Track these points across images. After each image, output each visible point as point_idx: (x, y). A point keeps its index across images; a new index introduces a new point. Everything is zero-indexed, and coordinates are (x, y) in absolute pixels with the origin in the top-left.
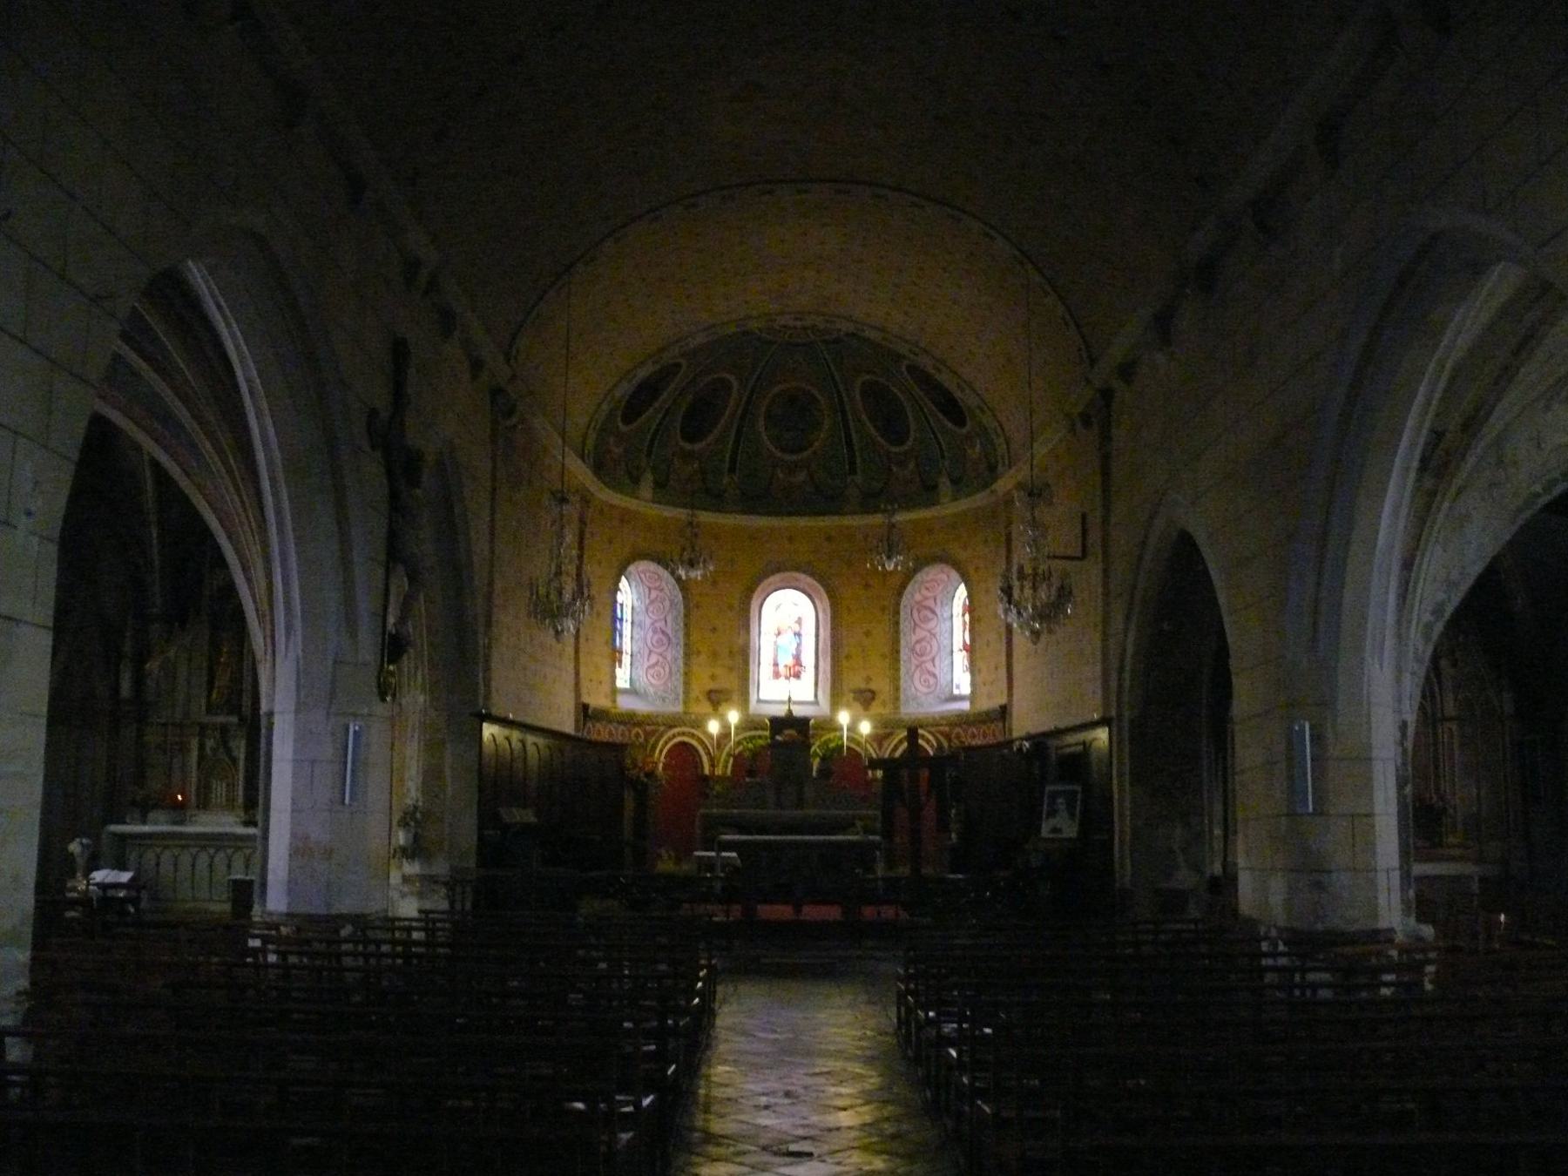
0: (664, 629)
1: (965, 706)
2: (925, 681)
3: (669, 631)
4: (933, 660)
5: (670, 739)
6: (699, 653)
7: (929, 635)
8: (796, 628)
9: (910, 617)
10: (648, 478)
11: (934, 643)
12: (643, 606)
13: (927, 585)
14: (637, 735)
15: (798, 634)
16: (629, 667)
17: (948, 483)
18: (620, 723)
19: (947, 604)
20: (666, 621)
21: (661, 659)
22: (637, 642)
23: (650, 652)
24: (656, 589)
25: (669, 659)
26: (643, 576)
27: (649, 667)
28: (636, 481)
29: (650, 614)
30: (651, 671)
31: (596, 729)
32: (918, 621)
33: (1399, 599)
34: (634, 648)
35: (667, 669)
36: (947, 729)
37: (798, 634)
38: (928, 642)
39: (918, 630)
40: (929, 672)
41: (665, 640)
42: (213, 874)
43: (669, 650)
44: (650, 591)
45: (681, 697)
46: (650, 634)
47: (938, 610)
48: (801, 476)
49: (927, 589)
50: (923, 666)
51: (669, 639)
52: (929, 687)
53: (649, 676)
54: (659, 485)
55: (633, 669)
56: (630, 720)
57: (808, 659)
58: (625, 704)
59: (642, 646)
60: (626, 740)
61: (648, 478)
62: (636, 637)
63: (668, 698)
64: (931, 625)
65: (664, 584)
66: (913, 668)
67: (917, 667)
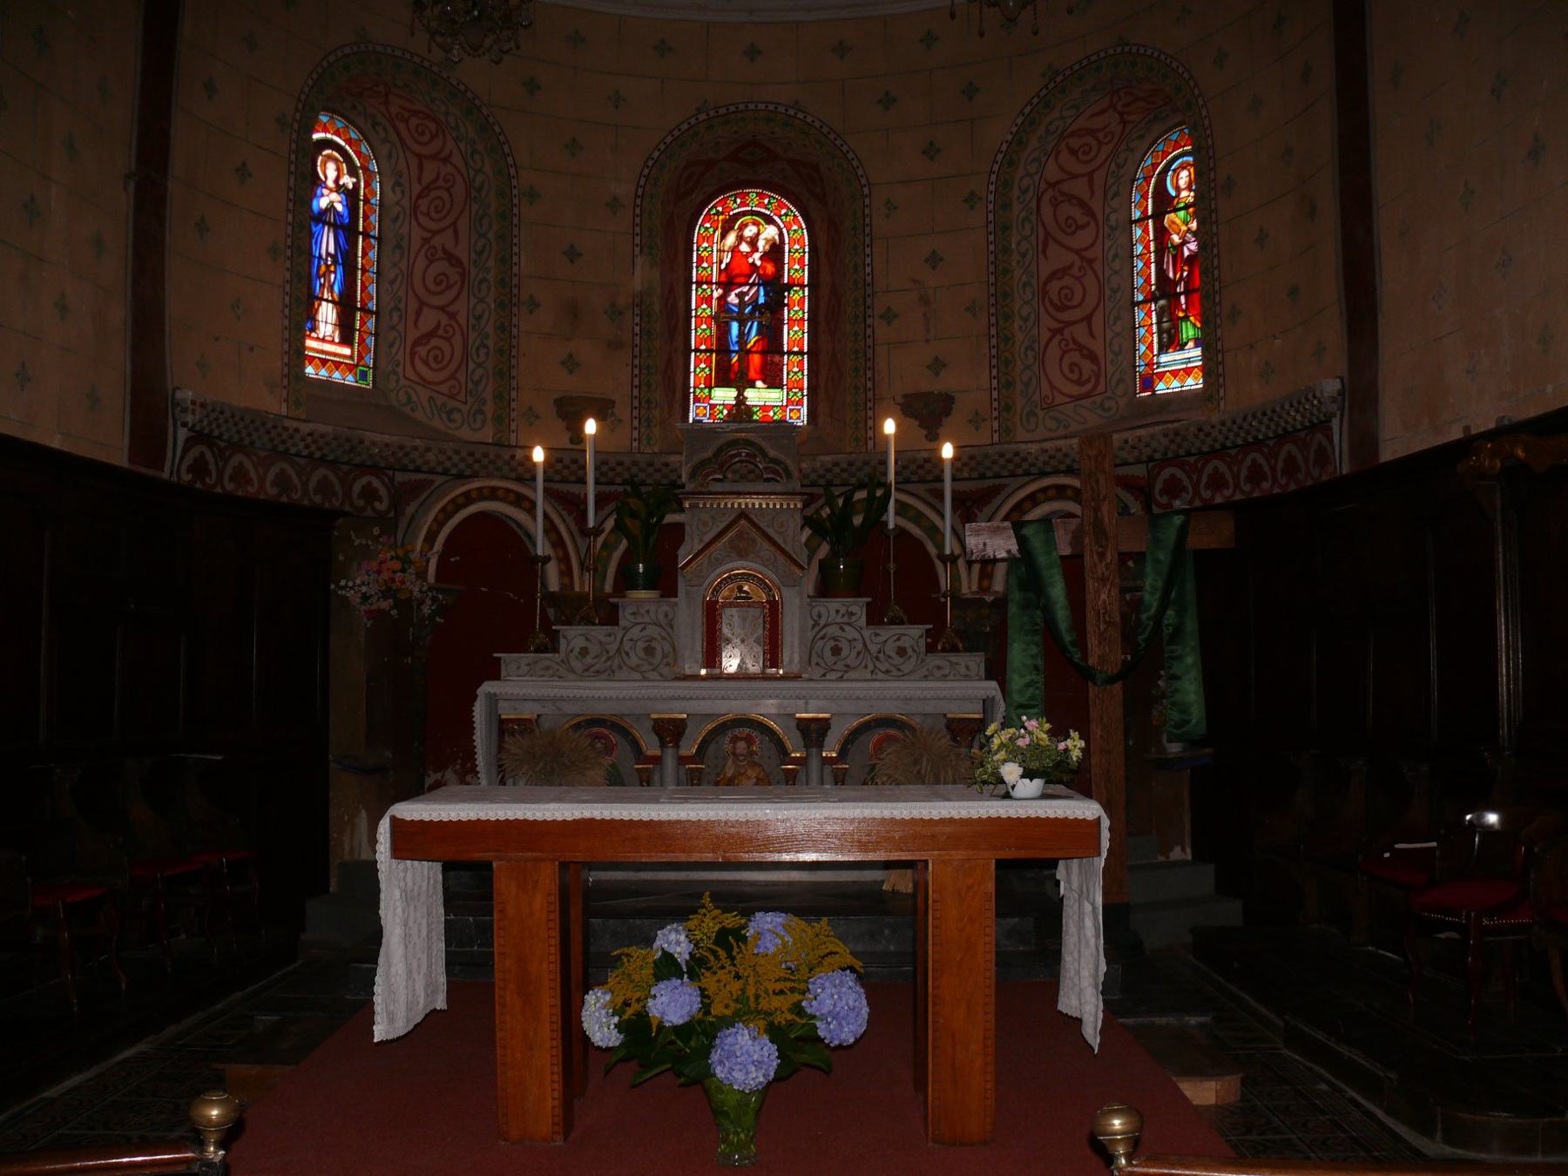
2: (1072, 371)
5: (456, 506)
6: (534, 305)
7: (1078, 263)
9: (1033, 218)
12: (405, 202)
13: (1075, 143)
14: (370, 494)
16: (371, 341)
19: (1116, 194)
20: (456, 232)
21: (445, 320)
22: (392, 282)
23: (422, 304)
24: (434, 157)
25: (462, 319)
26: (402, 126)
27: (417, 342)
29: (422, 219)
30: (422, 351)
31: (594, 661)
33: (438, 785)
35: (457, 340)
36: (1140, 471)
38: (1078, 279)
39: (1052, 247)
40: (1080, 347)
42: (700, 697)
44: (421, 167)
45: (489, 408)
46: (421, 263)
47: (1096, 205)
49: (1073, 152)
50: (1067, 332)
51: (463, 275)
52: (1079, 383)
53: (418, 362)
59: (402, 293)
63: (459, 411)
64: (1082, 239)
66: (1045, 335)
67: (1054, 332)
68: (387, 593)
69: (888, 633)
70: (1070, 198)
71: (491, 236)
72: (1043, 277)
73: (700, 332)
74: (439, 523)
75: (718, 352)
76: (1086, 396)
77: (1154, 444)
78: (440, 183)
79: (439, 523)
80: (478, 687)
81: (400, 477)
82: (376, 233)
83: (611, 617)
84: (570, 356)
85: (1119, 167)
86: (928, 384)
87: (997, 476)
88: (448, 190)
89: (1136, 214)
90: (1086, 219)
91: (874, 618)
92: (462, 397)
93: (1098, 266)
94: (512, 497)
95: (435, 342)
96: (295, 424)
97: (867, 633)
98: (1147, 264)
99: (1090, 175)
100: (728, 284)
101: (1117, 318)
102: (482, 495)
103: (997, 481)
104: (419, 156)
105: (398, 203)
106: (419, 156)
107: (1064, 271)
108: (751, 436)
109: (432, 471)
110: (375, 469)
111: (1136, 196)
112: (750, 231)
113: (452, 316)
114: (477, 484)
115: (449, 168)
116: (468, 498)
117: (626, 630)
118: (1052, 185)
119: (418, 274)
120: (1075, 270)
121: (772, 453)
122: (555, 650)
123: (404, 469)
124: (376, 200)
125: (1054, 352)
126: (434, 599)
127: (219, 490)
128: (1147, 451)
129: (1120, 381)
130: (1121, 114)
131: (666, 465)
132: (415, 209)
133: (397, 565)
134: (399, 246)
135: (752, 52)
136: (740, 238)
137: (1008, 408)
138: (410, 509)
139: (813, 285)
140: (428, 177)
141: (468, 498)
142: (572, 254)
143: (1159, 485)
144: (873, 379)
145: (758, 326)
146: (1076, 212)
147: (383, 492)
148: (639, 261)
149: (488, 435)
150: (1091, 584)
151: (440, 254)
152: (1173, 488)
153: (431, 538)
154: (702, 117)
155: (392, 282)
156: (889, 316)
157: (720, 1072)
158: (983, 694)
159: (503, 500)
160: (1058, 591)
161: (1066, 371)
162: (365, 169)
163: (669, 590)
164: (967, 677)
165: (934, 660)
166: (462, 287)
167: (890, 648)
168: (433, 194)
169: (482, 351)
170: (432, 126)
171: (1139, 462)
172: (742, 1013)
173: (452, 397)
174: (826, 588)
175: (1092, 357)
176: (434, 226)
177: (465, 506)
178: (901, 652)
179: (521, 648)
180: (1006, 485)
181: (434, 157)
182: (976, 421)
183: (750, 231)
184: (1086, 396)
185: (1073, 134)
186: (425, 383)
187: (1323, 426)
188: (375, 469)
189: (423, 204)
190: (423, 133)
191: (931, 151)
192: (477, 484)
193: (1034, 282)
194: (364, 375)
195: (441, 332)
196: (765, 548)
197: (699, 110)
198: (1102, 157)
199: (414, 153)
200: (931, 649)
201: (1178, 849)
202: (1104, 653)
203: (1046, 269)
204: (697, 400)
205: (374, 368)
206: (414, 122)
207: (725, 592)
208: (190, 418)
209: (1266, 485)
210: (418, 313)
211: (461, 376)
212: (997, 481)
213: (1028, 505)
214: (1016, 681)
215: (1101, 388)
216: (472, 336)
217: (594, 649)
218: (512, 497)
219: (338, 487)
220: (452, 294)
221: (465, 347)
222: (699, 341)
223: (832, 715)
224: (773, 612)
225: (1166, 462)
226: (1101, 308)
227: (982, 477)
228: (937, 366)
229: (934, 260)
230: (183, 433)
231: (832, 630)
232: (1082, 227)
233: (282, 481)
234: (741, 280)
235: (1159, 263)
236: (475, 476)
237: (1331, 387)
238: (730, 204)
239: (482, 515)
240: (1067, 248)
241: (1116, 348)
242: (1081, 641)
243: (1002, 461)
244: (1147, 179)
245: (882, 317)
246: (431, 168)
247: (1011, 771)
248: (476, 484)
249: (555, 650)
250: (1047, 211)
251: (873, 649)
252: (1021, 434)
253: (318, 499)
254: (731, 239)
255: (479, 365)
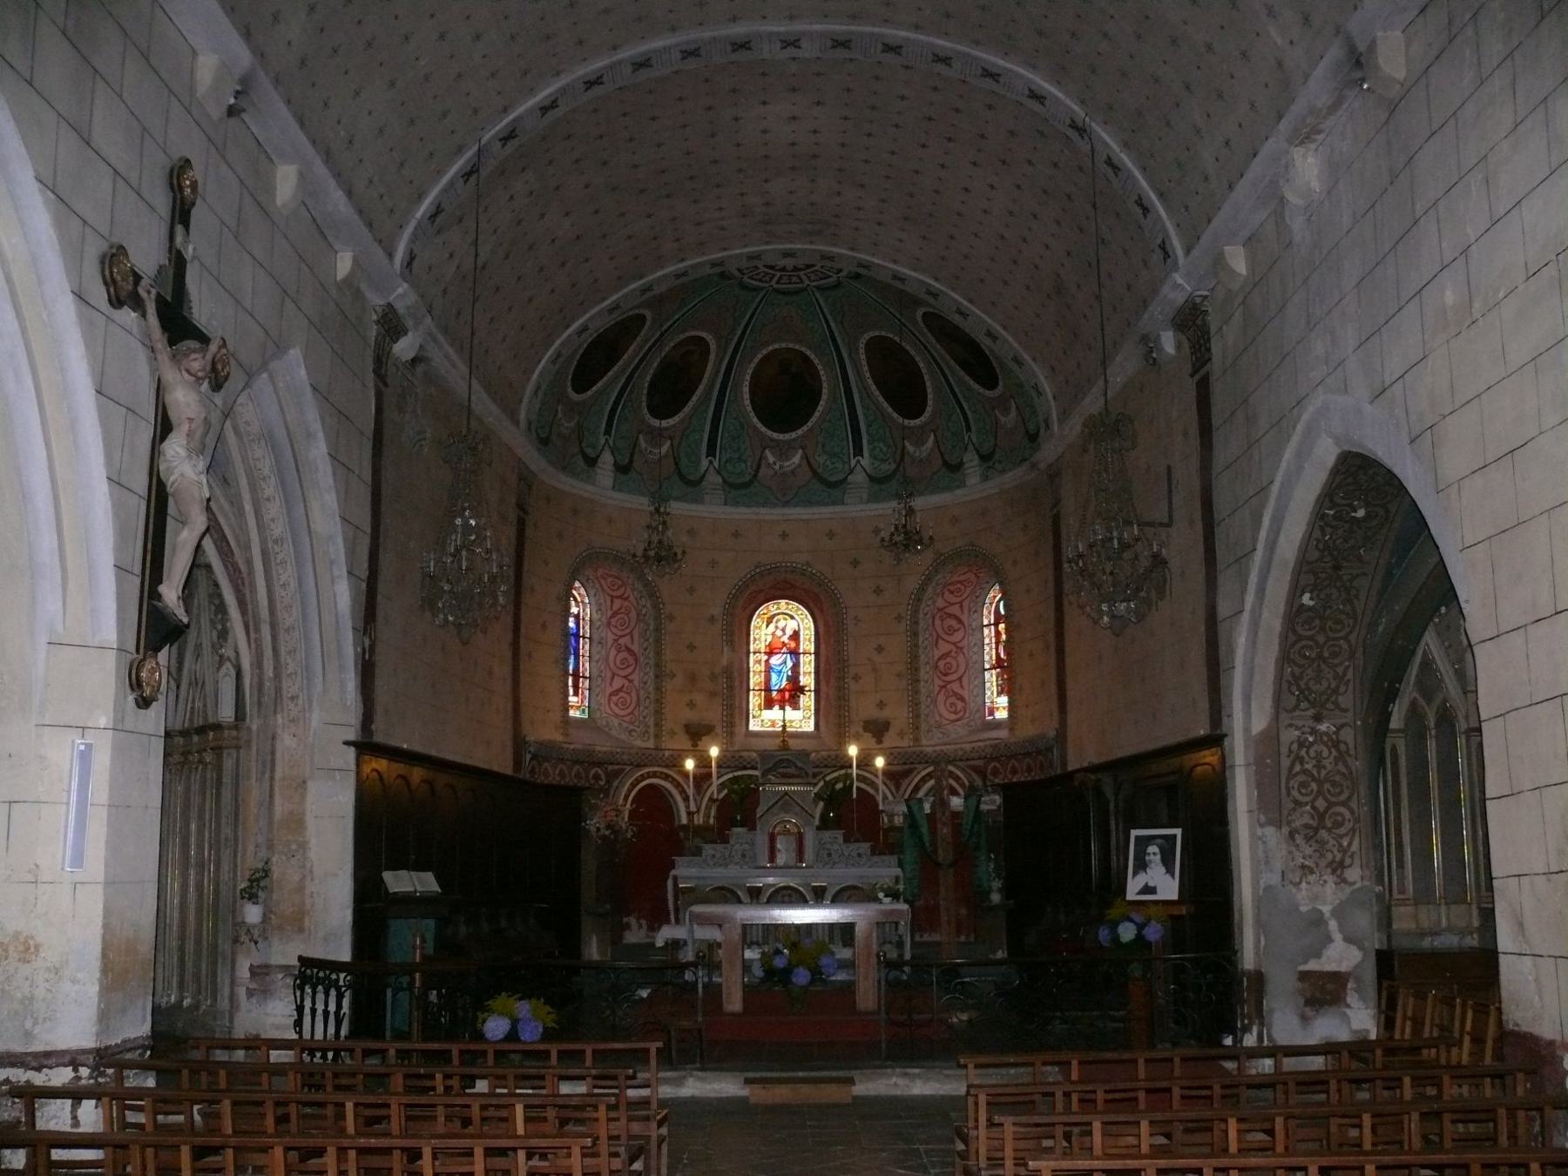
0: (629, 646)
1: (1003, 734)
3: (635, 648)
4: (960, 679)
5: (638, 781)
7: (955, 649)
8: (793, 645)
9: (931, 628)
10: (607, 459)
11: (961, 658)
12: (604, 619)
13: (952, 588)
14: (597, 777)
15: (795, 653)
16: (587, 693)
17: (976, 461)
18: (577, 762)
19: (975, 611)
20: (632, 637)
21: (627, 684)
22: (597, 662)
24: (617, 597)
25: (636, 683)
28: (592, 462)
30: (614, 699)
32: (940, 631)
34: (594, 670)
35: (634, 694)
36: (979, 763)
37: (795, 653)
38: (955, 658)
39: (941, 641)
40: (955, 694)
41: (631, 660)
43: (637, 671)
44: (612, 602)
45: (652, 730)
46: (613, 652)
47: (964, 618)
48: (796, 459)
49: (952, 592)
52: (955, 713)
53: (612, 705)
54: (622, 469)
55: (593, 697)
56: (588, 760)
57: (807, 680)
58: (581, 740)
60: (583, 783)
61: (607, 459)
62: (596, 657)
64: (956, 637)
65: (629, 592)
66: (937, 689)
68: (608, 827)
69: (854, 846)
70: (950, 615)
71: (651, 640)
72: (936, 658)
73: (755, 680)
74: (630, 791)
75: (765, 690)
76: (958, 720)
77: (987, 751)
78: (622, 611)
79: (630, 791)
80: (435, 876)
81: (610, 768)
82: (588, 635)
83: (725, 840)
84: (691, 701)
85: (977, 597)
86: (875, 714)
87: (912, 763)
88: (627, 614)
89: (985, 622)
90: (959, 626)
91: (846, 840)
92: (637, 724)
93: (965, 651)
94: (663, 776)
95: (621, 694)
96: (567, 746)
97: (844, 847)
98: (991, 649)
99: (961, 602)
100: (771, 652)
101: (975, 678)
102: (649, 775)
103: (912, 766)
104: (612, 597)
105: (600, 620)
106: (612, 597)
107: (947, 655)
108: (790, 758)
109: (625, 764)
110: (599, 764)
111: (985, 612)
112: (781, 624)
113: (631, 681)
114: (647, 770)
115: (626, 603)
116: (643, 778)
117: (733, 846)
118: (940, 610)
119: (611, 658)
120: (953, 654)
121: (800, 765)
122: (701, 856)
123: (612, 764)
124: (587, 618)
125: (941, 698)
126: (632, 830)
127: (539, 781)
128: (983, 754)
129: (977, 711)
130: (976, 575)
131: (741, 757)
132: (609, 624)
133: (614, 813)
134: (600, 643)
135: (784, 536)
136: (777, 627)
137: (918, 728)
138: (615, 784)
139: (817, 653)
140: (616, 607)
141: (643, 778)
142: (692, 647)
143: (989, 770)
144: (848, 711)
145: (831, 927)
146: (953, 623)
147: (603, 777)
148: (725, 649)
149: (651, 744)
150: (939, 826)
151: (623, 648)
152: (995, 772)
153: (626, 797)
154: (758, 570)
155: (597, 662)
156: (856, 678)
157: (794, 980)
158: (894, 874)
159: (659, 778)
160: (924, 830)
161: (948, 705)
162: (582, 602)
163: (752, 828)
164: (889, 867)
165: (875, 859)
166: (635, 668)
167: (854, 854)
168: (619, 616)
169: (648, 701)
170: (620, 583)
171: (979, 758)
172: (800, 963)
173: (632, 723)
174: (825, 824)
175: (962, 699)
176: (620, 633)
177: (642, 781)
178: (859, 855)
179: (681, 855)
180: (915, 768)
181: (617, 597)
182: (901, 734)
183: (781, 624)
184: (958, 720)
185: (950, 584)
186: (617, 716)
187: (1049, 749)
188: (599, 764)
189: (613, 621)
190: (614, 585)
191: (878, 591)
192: (647, 770)
193: (931, 662)
194: (584, 710)
195: (624, 689)
196: (797, 809)
197: (756, 567)
198: (968, 592)
199: (608, 594)
200: (873, 853)
201: (1000, 951)
202: (944, 855)
203: (937, 654)
204: (754, 717)
205: (589, 707)
206: (610, 580)
207: (778, 829)
208: (532, 749)
209: (1033, 774)
210: (612, 679)
211: (636, 713)
212: (912, 766)
213: (927, 778)
214: (908, 868)
215: (967, 715)
216: (642, 692)
217: (718, 855)
218: (663, 776)
219: (583, 775)
220: (630, 670)
221: (638, 695)
222: (755, 685)
223: (829, 884)
224: (800, 838)
225: (993, 759)
226: (966, 675)
227: (905, 763)
228: (881, 705)
229: (880, 649)
230: (528, 757)
231: (829, 846)
232: (957, 630)
233: (562, 774)
234: (777, 651)
235: (997, 649)
236: (645, 766)
237: (1052, 733)
238: (771, 608)
239: (651, 786)
240: (948, 642)
241: (975, 693)
242: (935, 851)
243: (915, 756)
244: (991, 604)
245: (853, 678)
246: (618, 603)
247: (881, 895)
248: (647, 770)
249: (701, 856)
250: (938, 622)
251: (846, 854)
252: (924, 742)
253: (576, 781)
254: (772, 626)
255: (646, 708)
